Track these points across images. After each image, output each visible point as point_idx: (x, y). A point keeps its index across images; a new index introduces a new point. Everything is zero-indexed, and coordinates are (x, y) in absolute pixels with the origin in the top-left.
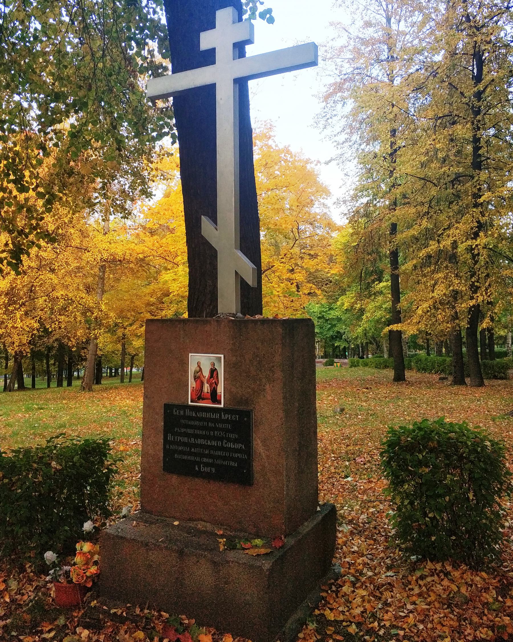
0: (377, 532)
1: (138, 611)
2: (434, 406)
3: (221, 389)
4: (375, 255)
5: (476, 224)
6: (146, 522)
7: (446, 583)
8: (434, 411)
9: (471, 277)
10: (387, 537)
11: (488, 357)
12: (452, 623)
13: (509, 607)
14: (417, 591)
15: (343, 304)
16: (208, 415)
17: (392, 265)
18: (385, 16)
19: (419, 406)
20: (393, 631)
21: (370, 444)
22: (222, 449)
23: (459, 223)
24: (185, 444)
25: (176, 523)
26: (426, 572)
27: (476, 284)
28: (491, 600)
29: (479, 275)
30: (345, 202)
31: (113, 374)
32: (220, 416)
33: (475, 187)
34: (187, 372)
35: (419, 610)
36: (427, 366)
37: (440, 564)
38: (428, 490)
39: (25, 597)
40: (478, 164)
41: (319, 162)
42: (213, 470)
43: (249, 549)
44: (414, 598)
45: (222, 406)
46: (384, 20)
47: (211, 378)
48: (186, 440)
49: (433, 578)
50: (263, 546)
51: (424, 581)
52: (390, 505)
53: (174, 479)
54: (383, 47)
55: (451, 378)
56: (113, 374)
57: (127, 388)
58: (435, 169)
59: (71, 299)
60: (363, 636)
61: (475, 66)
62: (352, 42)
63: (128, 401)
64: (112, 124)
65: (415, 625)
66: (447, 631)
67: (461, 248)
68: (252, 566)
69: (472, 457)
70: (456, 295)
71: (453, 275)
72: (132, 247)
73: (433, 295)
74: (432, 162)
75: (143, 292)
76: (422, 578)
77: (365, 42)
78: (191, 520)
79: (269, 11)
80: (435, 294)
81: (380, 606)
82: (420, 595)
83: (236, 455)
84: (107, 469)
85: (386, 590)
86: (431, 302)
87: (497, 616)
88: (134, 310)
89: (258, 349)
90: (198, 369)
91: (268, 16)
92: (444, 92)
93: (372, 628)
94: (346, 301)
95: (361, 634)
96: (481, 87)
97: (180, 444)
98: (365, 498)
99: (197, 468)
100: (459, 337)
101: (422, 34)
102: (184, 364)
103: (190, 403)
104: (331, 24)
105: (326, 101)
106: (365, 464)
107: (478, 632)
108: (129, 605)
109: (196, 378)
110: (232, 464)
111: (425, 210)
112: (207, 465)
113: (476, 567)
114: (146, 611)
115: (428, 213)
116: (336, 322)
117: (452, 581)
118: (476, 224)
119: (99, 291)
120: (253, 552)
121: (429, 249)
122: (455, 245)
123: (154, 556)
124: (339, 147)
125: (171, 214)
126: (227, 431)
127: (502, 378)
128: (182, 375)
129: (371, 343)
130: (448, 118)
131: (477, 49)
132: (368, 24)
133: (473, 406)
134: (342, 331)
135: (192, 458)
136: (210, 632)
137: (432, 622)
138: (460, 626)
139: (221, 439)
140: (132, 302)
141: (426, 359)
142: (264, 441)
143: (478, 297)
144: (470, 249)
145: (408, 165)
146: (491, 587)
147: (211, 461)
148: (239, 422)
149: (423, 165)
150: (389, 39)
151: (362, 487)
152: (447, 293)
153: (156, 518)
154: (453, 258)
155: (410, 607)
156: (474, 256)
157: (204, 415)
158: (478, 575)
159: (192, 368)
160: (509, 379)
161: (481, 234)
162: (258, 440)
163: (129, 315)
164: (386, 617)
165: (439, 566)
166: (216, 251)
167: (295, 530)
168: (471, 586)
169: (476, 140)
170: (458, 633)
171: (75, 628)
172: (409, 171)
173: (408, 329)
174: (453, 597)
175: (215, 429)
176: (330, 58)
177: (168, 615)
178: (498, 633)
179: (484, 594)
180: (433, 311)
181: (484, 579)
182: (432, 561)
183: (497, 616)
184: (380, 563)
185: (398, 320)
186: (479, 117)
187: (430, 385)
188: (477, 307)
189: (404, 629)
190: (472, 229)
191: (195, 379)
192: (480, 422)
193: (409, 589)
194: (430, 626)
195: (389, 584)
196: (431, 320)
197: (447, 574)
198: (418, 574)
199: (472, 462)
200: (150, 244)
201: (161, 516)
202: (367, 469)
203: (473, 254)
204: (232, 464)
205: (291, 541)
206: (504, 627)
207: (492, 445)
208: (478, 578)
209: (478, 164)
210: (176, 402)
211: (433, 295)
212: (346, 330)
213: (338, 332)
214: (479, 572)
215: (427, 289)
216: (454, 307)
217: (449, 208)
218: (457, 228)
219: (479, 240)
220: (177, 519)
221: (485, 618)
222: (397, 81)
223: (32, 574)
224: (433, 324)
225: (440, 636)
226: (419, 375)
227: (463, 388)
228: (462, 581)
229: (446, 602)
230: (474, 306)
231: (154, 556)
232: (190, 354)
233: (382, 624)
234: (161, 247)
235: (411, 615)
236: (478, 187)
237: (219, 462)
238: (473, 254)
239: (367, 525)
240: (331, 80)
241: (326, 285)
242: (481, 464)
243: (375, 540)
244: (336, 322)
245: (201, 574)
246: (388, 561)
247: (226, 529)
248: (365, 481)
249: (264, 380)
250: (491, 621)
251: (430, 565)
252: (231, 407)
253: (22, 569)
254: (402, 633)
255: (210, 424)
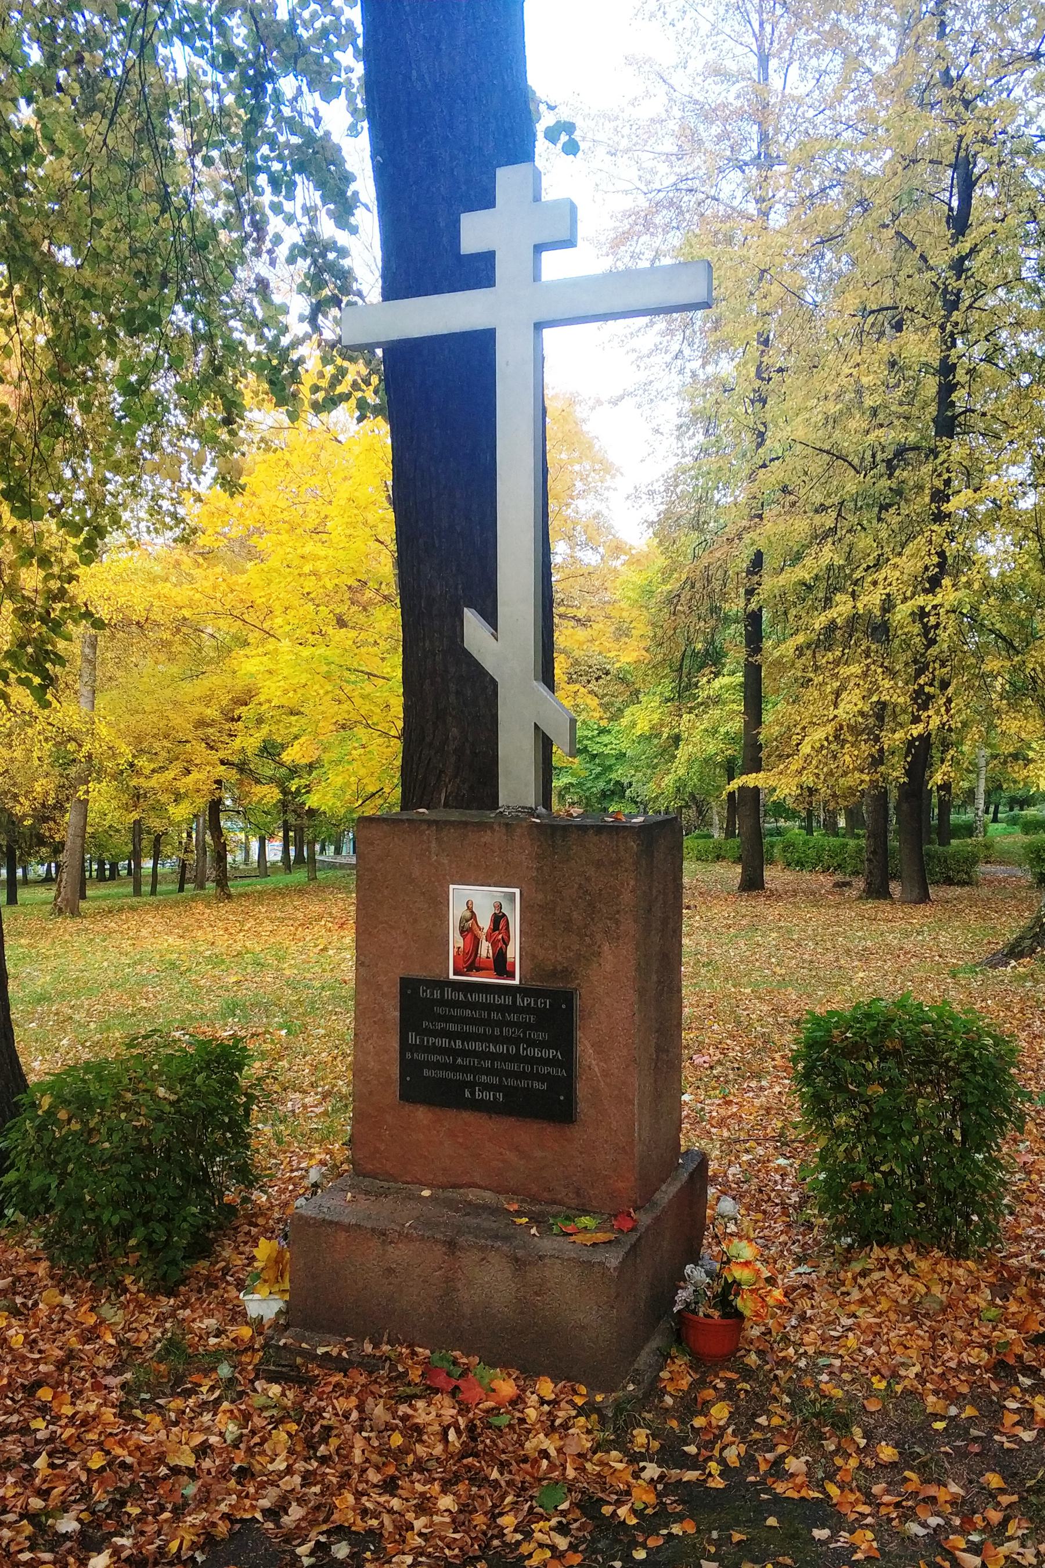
0: (766, 1198)
1: (368, 1348)
2: (829, 945)
3: (513, 952)
4: (719, 627)
5: (936, 560)
6: (367, 1193)
7: (906, 1280)
8: (831, 956)
9: (918, 676)
10: (784, 1206)
11: (934, 836)
12: (920, 1342)
13: (1013, 1314)
14: (856, 1295)
15: (634, 724)
16: (490, 999)
17: (748, 645)
18: (755, 50)
19: (799, 945)
20: (822, 1361)
21: (716, 1027)
22: (517, 1058)
23: (900, 554)
24: (442, 1051)
25: (426, 1193)
26: (871, 1264)
27: (927, 689)
28: (983, 1304)
29: (934, 669)
30: (651, 493)
31: (107, 873)
32: (514, 1001)
33: (940, 475)
34: (444, 918)
35: (863, 1325)
36: (807, 856)
37: (895, 1250)
38: (882, 1125)
39: (144, 1336)
40: (948, 425)
41: (599, 402)
42: (500, 1096)
43: (575, 1234)
44: (853, 1307)
45: (517, 982)
46: (754, 60)
47: (494, 930)
48: (444, 1042)
49: (882, 1274)
50: (598, 1229)
51: (868, 1280)
52: (776, 1148)
53: (422, 1114)
54: (748, 128)
55: (860, 883)
56: (107, 873)
57: (157, 908)
58: (855, 436)
59: (31, 713)
60: (772, 1370)
61: (955, 190)
62: (677, 113)
63: (170, 940)
64: (211, 362)
65: (860, 1350)
66: (915, 1356)
67: (902, 612)
68: (590, 1264)
69: (964, 1067)
70: (882, 711)
71: (879, 670)
72: (166, 591)
73: (836, 712)
74: (852, 416)
75: (185, 694)
76: (864, 1273)
77: (708, 114)
78: (455, 1186)
79: (569, 128)
80: (839, 712)
81: (794, 1322)
82: (862, 1302)
83: (545, 1070)
84: (246, 1095)
85: (802, 1296)
86: (830, 728)
87: (994, 1329)
88: (166, 737)
89: (588, 879)
90: (468, 914)
91: (564, 138)
92: (885, 256)
93: (784, 1358)
94: (644, 716)
95: (767, 1367)
96: (966, 246)
97: (434, 1050)
98: (726, 1134)
99: (467, 1094)
100: (882, 797)
101: (837, 95)
102: (440, 904)
103: (452, 976)
104: (629, 61)
105: (615, 254)
106: (711, 1068)
107: (964, 1355)
108: (348, 1339)
109: (463, 931)
110: (537, 1085)
111: (830, 523)
112: (486, 1087)
113: (959, 1252)
114: (386, 1348)
115: (833, 530)
116: (613, 761)
117: (916, 1277)
118: (936, 560)
119: (85, 691)
120: (588, 1239)
121: (832, 613)
122: (888, 605)
123: (399, 1253)
124: (642, 365)
125: (258, 517)
126: (527, 1026)
127: (963, 884)
128: (434, 925)
129: (687, 806)
130: (890, 313)
131: (962, 154)
132: (718, 72)
133: (908, 946)
134: (625, 781)
135: (459, 1076)
136: (510, 1375)
137: (887, 1342)
138: (934, 1347)
139: (516, 1041)
140: (162, 717)
141: (805, 843)
142: (598, 1046)
143: (929, 717)
144: (921, 614)
145: (798, 421)
146: (983, 1285)
147: (495, 1081)
148: (551, 1011)
149: (832, 421)
150: (761, 112)
151: (714, 1114)
152: (866, 709)
153: (385, 1184)
154: (880, 630)
155: (847, 1322)
156: (926, 629)
157: (482, 998)
158: (960, 1266)
159: (456, 912)
160: (977, 885)
161: (946, 582)
162: (586, 1042)
163: (157, 746)
164: (807, 1339)
165: (893, 1254)
166: (494, 683)
167: (649, 1200)
168: (950, 1284)
169: (947, 369)
170: (933, 1358)
171: (252, 1382)
172: (800, 434)
173: (778, 783)
174: (920, 1303)
175: (501, 1024)
176: (627, 151)
177: (428, 1352)
178: (998, 1353)
179: (972, 1296)
180: (833, 747)
181: (970, 1272)
182: (880, 1245)
183: (994, 1329)
184: (782, 1251)
185: (755, 765)
186: (956, 316)
187: (814, 898)
188: (925, 739)
189: (841, 1357)
190: (926, 568)
191: (462, 932)
192: (927, 980)
193: (842, 1294)
194: (884, 1349)
195: (806, 1286)
196: (826, 764)
197: (907, 1266)
198: (857, 1267)
199: (962, 1076)
200: (206, 584)
201: (396, 1181)
202: (718, 1078)
203: (925, 626)
204: (537, 1085)
205: (644, 1219)
206: (1008, 1344)
207: (996, 1044)
208: (961, 1271)
209: (948, 425)
210: (422, 974)
211: (836, 712)
212: (635, 779)
213: (618, 783)
214: (961, 1261)
215: (824, 699)
216: (877, 739)
217: (880, 520)
218: (895, 566)
219: (940, 596)
220: (429, 1186)
221: (975, 1333)
222: (778, 219)
223: (142, 1295)
224: (831, 773)
225: (903, 1364)
226: (789, 876)
227: (885, 905)
228: (933, 1277)
229: (907, 1311)
230: (920, 736)
231: (399, 1253)
232: (452, 887)
233: (801, 1351)
234: (232, 591)
235: (850, 1334)
236: (946, 476)
237: (511, 1082)
238: (925, 626)
239: (745, 1186)
240: (627, 203)
241: (597, 679)
242: (978, 1078)
243: (764, 1212)
244: (613, 761)
245: (489, 1282)
246: (795, 1248)
247: (525, 1201)
248: (717, 1102)
249: (598, 936)
250: (985, 1337)
251: (877, 1252)
252: (537, 984)
253: (120, 1288)
254: (837, 1362)
255: (494, 1015)
